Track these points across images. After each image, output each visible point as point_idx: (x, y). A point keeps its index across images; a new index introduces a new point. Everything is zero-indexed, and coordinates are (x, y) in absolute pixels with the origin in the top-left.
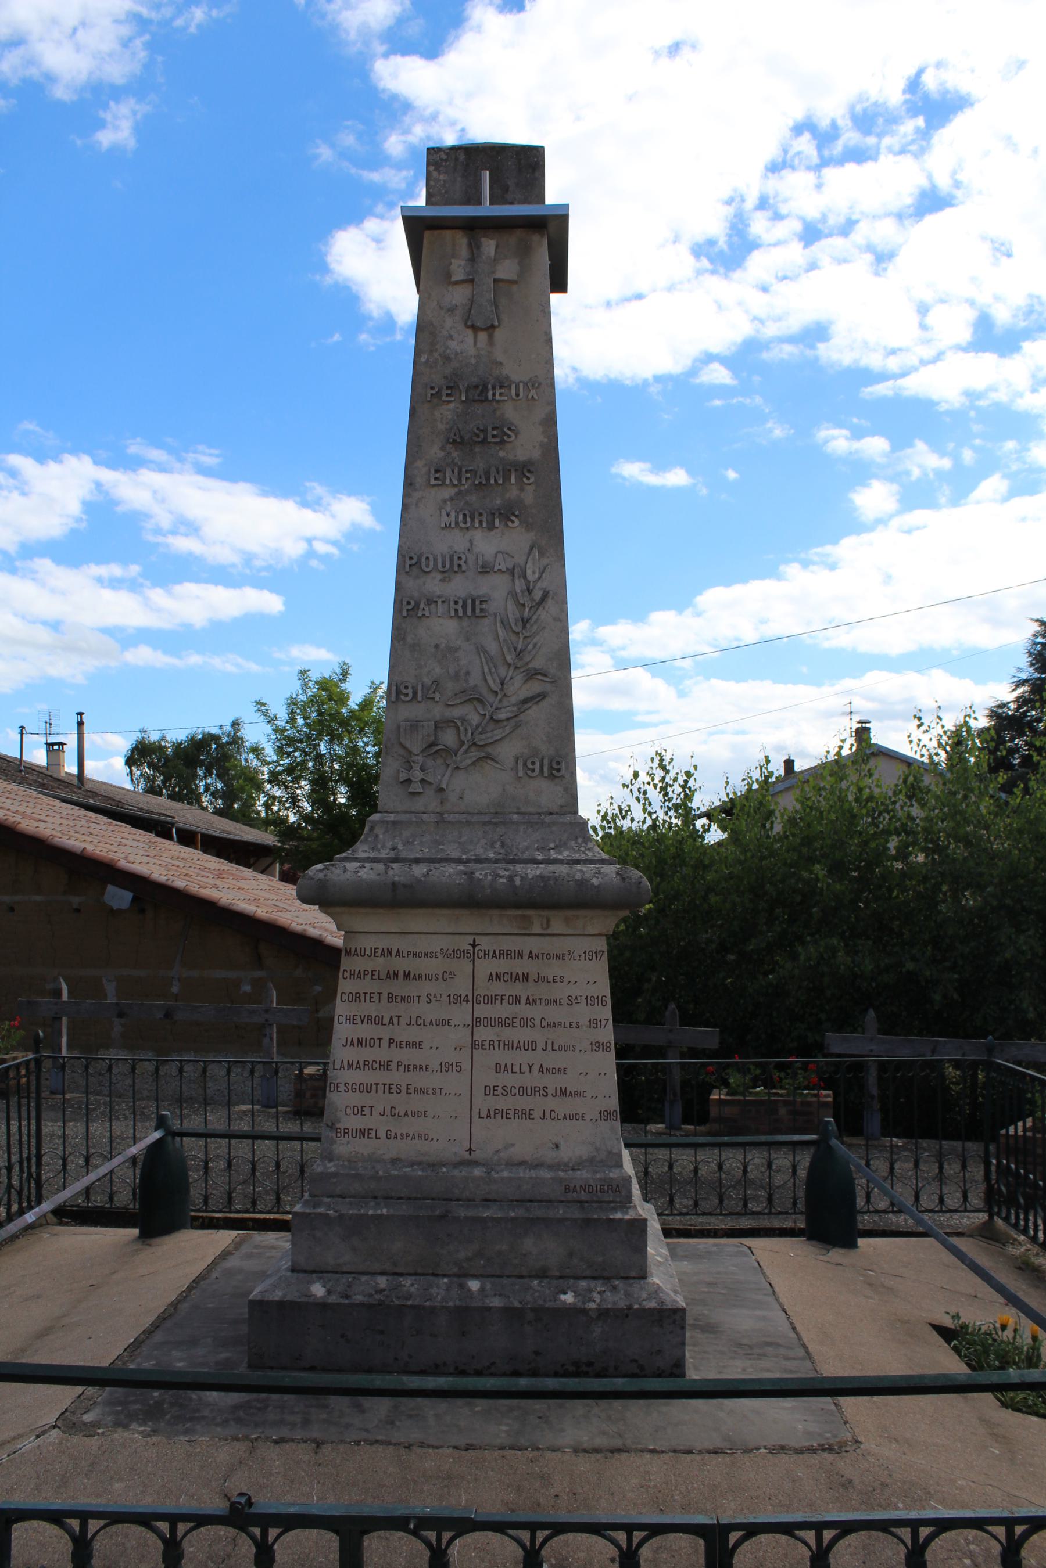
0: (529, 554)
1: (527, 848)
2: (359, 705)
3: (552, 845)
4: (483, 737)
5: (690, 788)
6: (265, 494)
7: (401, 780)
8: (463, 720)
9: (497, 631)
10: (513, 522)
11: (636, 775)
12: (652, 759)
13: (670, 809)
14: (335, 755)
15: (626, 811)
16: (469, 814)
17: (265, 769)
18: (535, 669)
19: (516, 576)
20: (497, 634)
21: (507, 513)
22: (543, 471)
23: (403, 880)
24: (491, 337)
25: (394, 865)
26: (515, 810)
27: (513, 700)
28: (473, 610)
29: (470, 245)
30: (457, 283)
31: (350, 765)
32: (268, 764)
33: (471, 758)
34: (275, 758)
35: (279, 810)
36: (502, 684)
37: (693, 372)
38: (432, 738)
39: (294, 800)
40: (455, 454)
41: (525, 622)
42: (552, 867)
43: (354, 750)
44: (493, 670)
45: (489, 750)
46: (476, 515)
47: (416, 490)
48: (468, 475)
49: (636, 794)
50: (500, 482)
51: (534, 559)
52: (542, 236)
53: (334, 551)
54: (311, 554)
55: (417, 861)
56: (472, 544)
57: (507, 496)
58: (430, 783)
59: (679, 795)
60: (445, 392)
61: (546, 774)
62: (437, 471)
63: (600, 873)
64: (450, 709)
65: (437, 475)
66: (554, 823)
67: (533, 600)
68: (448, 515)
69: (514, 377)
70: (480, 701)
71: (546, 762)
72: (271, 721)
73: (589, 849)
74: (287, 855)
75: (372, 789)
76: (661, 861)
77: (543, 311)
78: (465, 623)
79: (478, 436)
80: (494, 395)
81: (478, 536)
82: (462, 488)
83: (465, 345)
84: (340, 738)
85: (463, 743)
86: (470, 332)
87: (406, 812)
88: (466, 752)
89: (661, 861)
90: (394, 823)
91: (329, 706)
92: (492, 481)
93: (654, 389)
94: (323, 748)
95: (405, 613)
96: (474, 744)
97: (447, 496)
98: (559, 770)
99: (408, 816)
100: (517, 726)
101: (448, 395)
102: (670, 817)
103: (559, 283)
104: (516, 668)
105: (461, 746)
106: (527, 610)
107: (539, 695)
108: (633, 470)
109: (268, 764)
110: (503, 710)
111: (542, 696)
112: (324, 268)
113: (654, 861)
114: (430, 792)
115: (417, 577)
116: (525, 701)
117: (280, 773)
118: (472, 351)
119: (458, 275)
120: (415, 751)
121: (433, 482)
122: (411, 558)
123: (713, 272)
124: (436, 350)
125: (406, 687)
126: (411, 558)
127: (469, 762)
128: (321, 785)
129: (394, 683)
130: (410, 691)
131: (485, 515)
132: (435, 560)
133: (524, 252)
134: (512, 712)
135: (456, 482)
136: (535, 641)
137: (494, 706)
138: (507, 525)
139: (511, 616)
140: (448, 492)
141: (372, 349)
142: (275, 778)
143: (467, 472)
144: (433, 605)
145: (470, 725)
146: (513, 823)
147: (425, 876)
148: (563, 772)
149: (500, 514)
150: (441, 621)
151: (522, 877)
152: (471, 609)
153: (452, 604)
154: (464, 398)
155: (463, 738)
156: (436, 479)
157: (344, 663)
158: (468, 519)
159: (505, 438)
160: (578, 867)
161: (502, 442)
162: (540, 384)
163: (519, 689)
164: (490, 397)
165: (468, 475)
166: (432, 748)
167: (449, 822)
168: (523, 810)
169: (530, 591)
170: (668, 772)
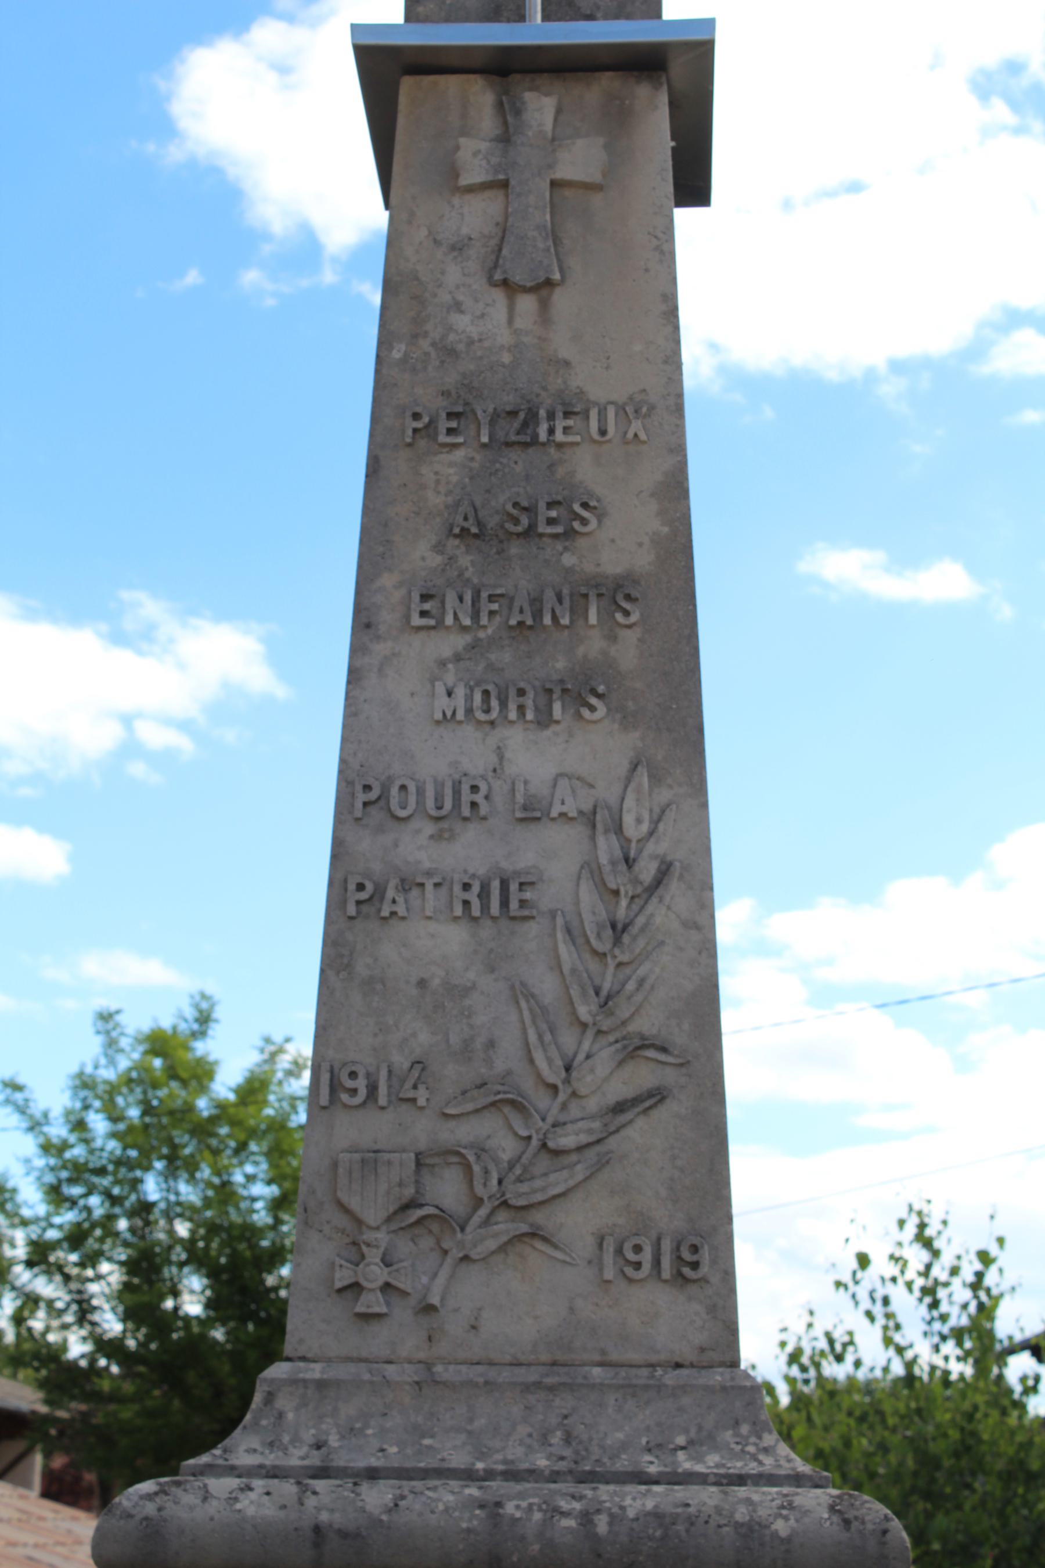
0: (628, 780)
1: (624, 1446)
2: (238, 1091)
3: (681, 1440)
4: (524, 1188)
5: (988, 1291)
6: (30, 615)
7: (338, 1285)
8: (481, 1150)
9: (556, 949)
10: (592, 709)
11: (863, 1260)
12: (901, 1223)
13: (944, 1338)
14: (179, 1204)
15: (845, 1345)
16: (491, 1364)
17: (20, 1236)
18: (643, 1037)
19: (600, 826)
20: (558, 957)
21: (580, 691)
22: (660, 598)
23: (338, 1519)
24: (544, 305)
25: (320, 1485)
26: (597, 1358)
27: (592, 1104)
28: (505, 903)
29: (500, 106)
30: (470, 189)
31: (213, 1229)
32: (25, 1223)
33: (495, 1236)
34: (42, 1209)
35: (48, 1329)
36: (568, 1069)
37: (976, 350)
38: (409, 1192)
39: (84, 1310)
40: (465, 561)
41: (618, 930)
42: (680, 1493)
43: (225, 1193)
44: (548, 1037)
45: (538, 1217)
46: (512, 693)
47: (378, 638)
48: (495, 607)
49: (865, 1304)
50: (565, 621)
51: (638, 791)
52: (657, 87)
53: (183, 743)
54: (130, 749)
55: (373, 1474)
56: (501, 758)
57: (581, 651)
58: (404, 1294)
59: (965, 1306)
60: (443, 424)
61: (666, 1274)
62: (425, 597)
63: (791, 1506)
64: (452, 1124)
65: (427, 606)
66: (685, 1388)
67: (636, 881)
68: (449, 694)
69: (596, 393)
70: (517, 1106)
71: (667, 1246)
72: (35, 1126)
73: (766, 1450)
74: (61, 1433)
75: (262, 1282)
76: (928, 1462)
77: (658, 249)
78: (487, 930)
79: (516, 521)
80: (551, 431)
81: (516, 739)
82: (481, 634)
83: (490, 323)
84: (191, 1167)
85: (479, 1202)
86: (499, 296)
87: (350, 1359)
88: (487, 1222)
89: (928, 1462)
90: (321, 1385)
91: (171, 1092)
92: (547, 620)
93: (889, 389)
94: (152, 1188)
95: (352, 910)
96: (505, 1204)
97: (447, 652)
98: (695, 1266)
99: (352, 1368)
100: (602, 1164)
101: (450, 431)
102: (946, 1358)
103: (693, 185)
104: (599, 1032)
105: (475, 1209)
106: (624, 903)
107: (650, 1094)
108: (847, 568)
109: (25, 1223)
110: (569, 1127)
111: (656, 1096)
112: (166, 129)
113: (910, 1463)
114: (402, 1313)
115: (380, 829)
116: (619, 1108)
117: (54, 1246)
118: (505, 337)
119: (474, 173)
120: (372, 1215)
121: (417, 621)
122: (367, 788)
123: (1019, 130)
124: (426, 334)
125: (353, 1075)
126: (367, 788)
127: (492, 1244)
128: (146, 1271)
129: (326, 1066)
130: (361, 1084)
131: (531, 694)
132: (420, 792)
133: (618, 121)
134: (590, 1131)
135: (467, 622)
136: (641, 971)
137: (550, 1120)
138: (579, 716)
139: (588, 918)
140: (451, 643)
141: (270, 302)
142: (39, 1256)
143: (491, 598)
144: (415, 892)
145: (496, 1161)
146: (593, 1386)
147: (389, 1511)
148: (704, 1269)
149: (565, 691)
150: (432, 926)
151: (612, 1516)
152: (500, 900)
153: (457, 889)
154: (485, 439)
155: (479, 1190)
156: (423, 614)
157: (204, 996)
158: (494, 703)
159: (576, 525)
160: (742, 1492)
161: (570, 534)
162: (652, 408)
163: (606, 1079)
164: (543, 436)
165: (495, 607)
166: (410, 1212)
167: (444, 1383)
168: (614, 1356)
169: (629, 862)
170: (936, 1254)
